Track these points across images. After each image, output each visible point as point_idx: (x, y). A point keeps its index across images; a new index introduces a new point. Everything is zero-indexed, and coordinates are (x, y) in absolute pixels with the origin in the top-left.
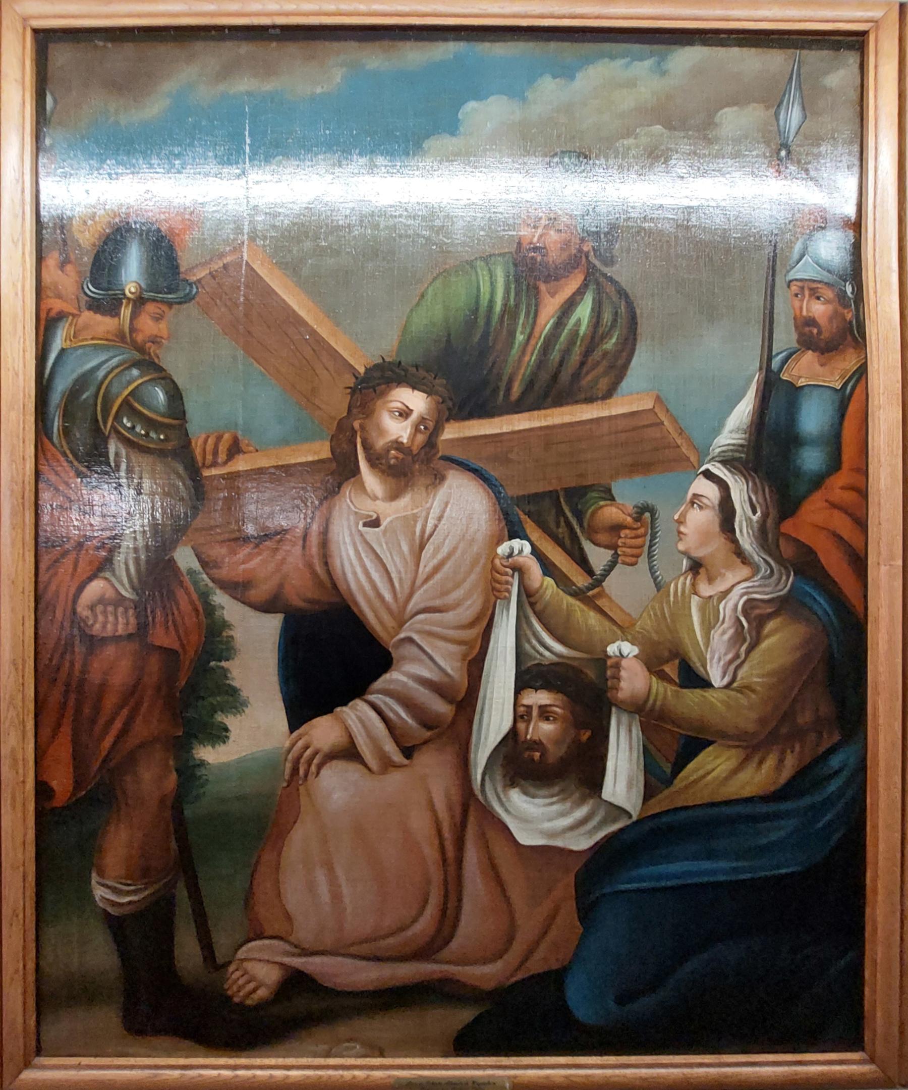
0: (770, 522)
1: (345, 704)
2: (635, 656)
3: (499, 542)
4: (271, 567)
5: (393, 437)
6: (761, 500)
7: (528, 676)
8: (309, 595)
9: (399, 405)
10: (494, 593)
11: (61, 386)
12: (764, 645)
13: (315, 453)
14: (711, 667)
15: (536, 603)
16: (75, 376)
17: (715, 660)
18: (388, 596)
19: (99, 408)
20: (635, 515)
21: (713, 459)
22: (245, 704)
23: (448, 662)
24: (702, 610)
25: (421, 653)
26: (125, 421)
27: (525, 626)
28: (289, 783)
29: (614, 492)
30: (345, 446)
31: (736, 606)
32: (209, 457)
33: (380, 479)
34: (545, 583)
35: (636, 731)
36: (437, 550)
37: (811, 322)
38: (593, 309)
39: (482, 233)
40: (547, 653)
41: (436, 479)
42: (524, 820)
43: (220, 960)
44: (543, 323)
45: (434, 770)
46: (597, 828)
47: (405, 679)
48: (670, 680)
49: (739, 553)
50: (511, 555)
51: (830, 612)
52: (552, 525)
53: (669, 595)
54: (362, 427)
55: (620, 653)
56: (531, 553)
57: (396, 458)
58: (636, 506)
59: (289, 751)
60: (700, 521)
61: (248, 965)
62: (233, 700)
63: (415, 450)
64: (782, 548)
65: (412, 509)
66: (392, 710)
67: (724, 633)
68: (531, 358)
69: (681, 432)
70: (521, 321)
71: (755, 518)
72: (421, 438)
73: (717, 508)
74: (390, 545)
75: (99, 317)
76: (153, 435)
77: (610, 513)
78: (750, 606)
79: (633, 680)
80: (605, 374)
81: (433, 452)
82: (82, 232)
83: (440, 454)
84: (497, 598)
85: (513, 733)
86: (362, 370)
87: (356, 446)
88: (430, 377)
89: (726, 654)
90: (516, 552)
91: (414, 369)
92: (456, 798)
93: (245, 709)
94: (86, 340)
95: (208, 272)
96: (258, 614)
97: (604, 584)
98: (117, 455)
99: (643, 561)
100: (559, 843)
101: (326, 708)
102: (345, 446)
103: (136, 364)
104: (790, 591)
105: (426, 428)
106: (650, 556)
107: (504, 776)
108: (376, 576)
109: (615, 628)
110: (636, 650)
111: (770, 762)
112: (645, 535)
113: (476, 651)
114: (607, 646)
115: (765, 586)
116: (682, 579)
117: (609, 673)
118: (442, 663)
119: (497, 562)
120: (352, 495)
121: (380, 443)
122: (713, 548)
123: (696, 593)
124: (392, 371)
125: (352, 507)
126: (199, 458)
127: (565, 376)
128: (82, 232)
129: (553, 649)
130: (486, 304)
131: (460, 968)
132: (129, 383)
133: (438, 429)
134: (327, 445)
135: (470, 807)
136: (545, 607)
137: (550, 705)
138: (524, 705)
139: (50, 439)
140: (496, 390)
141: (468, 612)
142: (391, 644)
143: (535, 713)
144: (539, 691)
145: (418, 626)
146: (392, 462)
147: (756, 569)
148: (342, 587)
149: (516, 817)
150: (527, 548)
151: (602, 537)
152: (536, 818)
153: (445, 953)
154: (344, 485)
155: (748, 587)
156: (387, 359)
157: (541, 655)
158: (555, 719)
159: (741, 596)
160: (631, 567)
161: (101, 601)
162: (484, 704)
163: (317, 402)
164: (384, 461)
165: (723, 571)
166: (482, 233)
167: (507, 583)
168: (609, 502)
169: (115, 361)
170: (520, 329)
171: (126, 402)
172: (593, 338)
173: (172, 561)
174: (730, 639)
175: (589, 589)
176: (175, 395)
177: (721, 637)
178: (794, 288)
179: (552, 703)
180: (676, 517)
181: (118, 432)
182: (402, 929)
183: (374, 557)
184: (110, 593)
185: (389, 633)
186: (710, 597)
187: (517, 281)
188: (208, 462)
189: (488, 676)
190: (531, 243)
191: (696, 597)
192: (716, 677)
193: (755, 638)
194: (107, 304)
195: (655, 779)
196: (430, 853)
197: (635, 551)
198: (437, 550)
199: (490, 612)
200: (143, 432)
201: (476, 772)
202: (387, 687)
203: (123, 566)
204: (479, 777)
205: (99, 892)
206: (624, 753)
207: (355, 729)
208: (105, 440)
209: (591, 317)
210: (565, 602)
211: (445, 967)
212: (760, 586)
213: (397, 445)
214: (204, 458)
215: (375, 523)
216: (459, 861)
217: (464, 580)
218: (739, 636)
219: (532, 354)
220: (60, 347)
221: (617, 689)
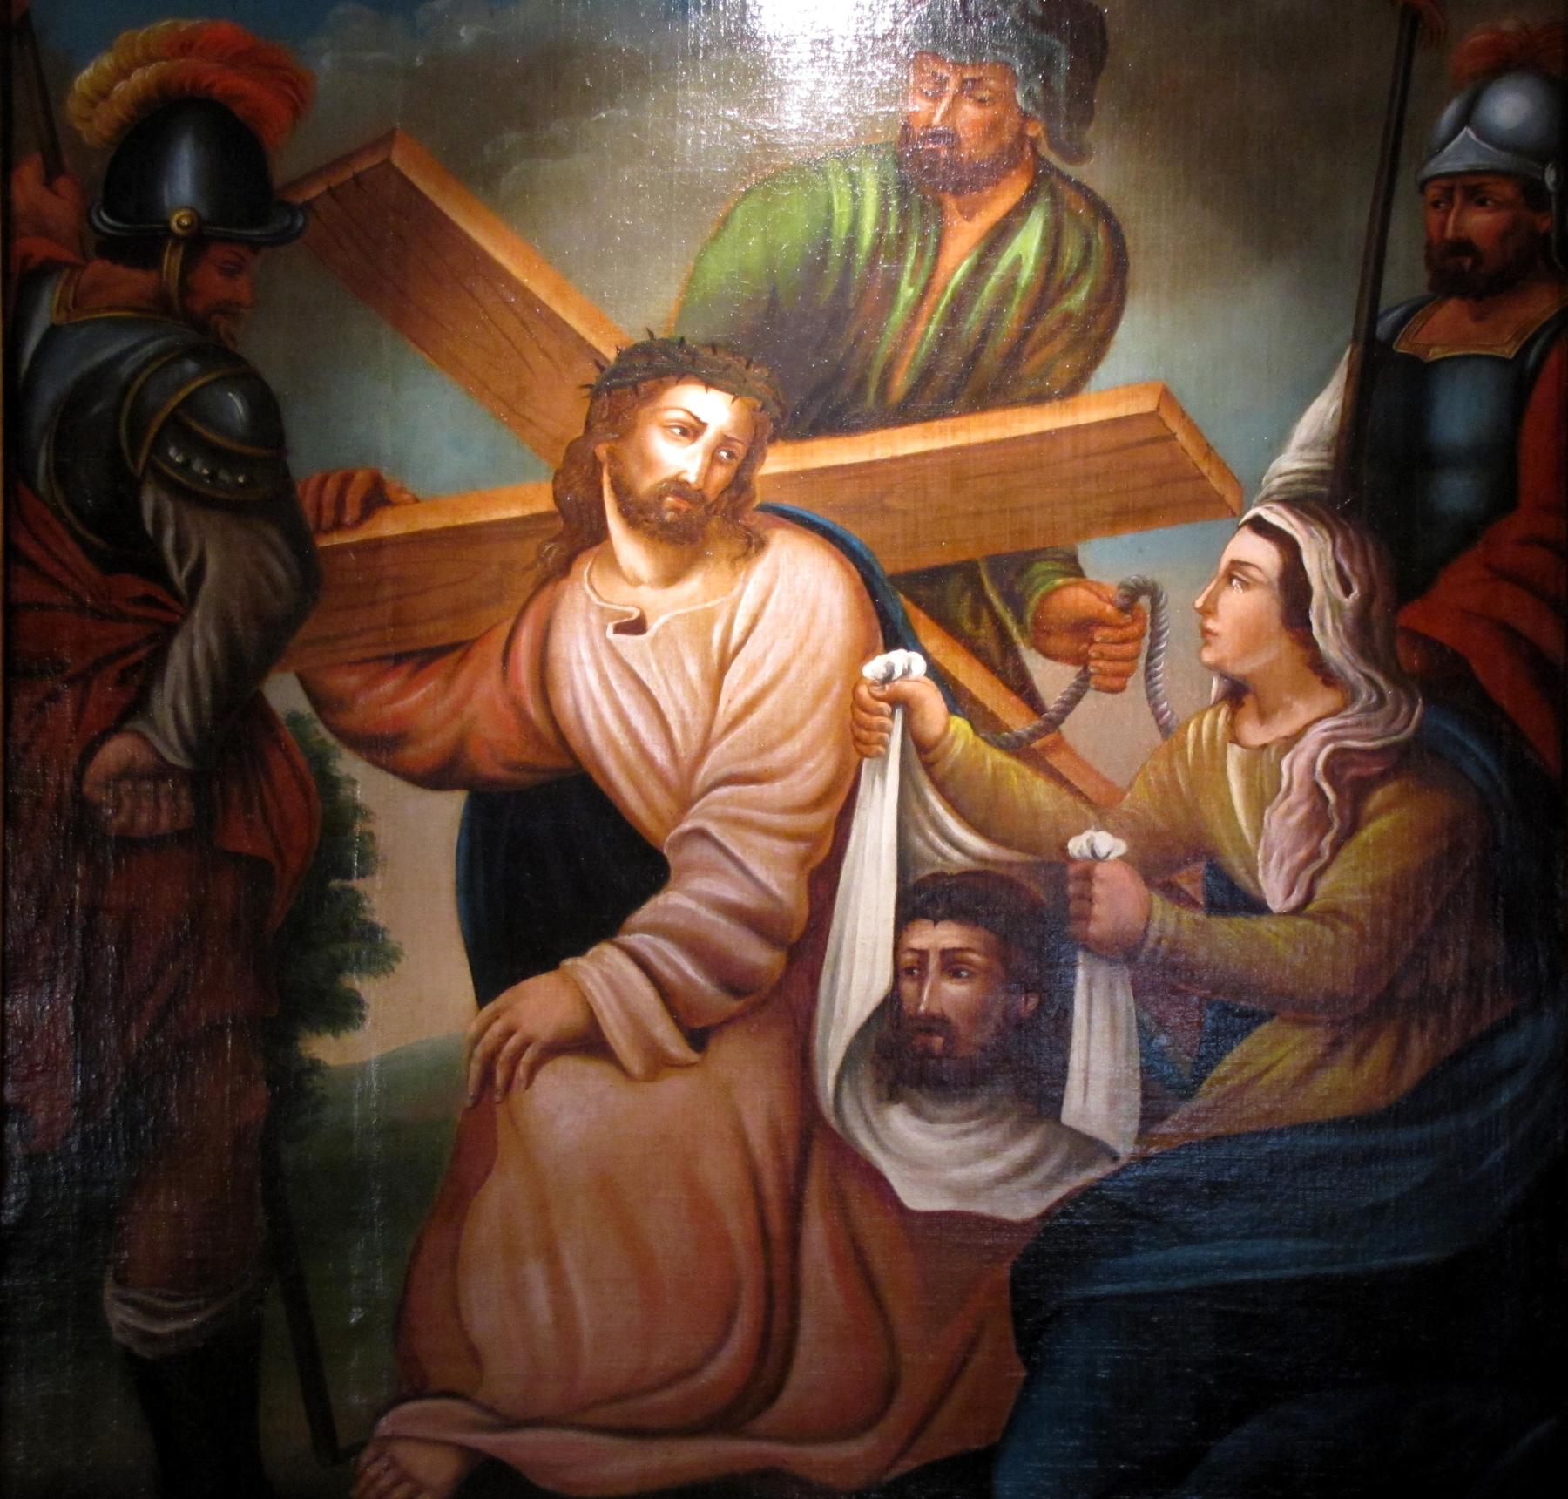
0: (1376, 609)
1: (580, 951)
2: (1121, 858)
3: (867, 654)
4: (443, 706)
5: (670, 472)
6: (1359, 568)
7: (919, 897)
8: (515, 757)
9: (680, 415)
10: (857, 743)
11: (49, 393)
12: (1367, 834)
13: (524, 504)
14: (1265, 874)
15: (932, 764)
16: (75, 374)
17: (1273, 862)
18: (660, 756)
19: (123, 430)
20: (1120, 601)
21: (1267, 498)
22: (395, 955)
23: (773, 874)
24: (1248, 770)
25: (721, 858)
26: (172, 452)
27: (915, 806)
28: (478, 1100)
29: (1082, 563)
30: (579, 489)
31: (1313, 761)
32: (328, 515)
33: (646, 545)
34: (953, 728)
35: (1124, 998)
36: (753, 670)
37: (1463, 246)
38: (1044, 240)
39: (836, 110)
40: (956, 855)
41: (750, 545)
42: (916, 1164)
43: (344, 1440)
44: (950, 266)
45: (745, 1074)
46: (1052, 1180)
47: (692, 905)
48: (1193, 903)
49: (1318, 666)
50: (888, 679)
51: (1495, 771)
52: (968, 626)
53: (1184, 746)
54: (612, 456)
55: (1093, 853)
56: (927, 675)
57: (676, 510)
58: (1122, 586)
59: (476, 1041)
60: (1241, 607)
61: (401, 1451)
62: (376, 951)
63: (711, 493)
64: (1402, 654)
65: (706, 601)
66: (669, 962)
67: (1290, 811)
68: (930, 329)
69: (1209, 452)
70: (909, 265)
71: (1348, 602)
72: (721, 474)
73: (1276, 584)
74: (666, 666)
75: (120, 271)
76: (224, 476)
77: (1076, 599)
78: (1338, 762)
79: (1118, 900)
80: (1068, 350)
81: (744, 497)
82: (88, 120)
83: (758, 502)
84: (863, 755)
85: (891, 1005)
86: (611, 355)
87: (601, 496)
88: (738, 364)
89: (1294, 850)
90: (898, 673)
91: (709, 352)
92: (787, 1125)
93: (394, 964)
94: (98, 310)
95: (323, 188)
96: (418, 792)
97: (1063, 727)
98: (158, 512)
99: (1136, 682)
100: (981, 1207)
101: (546, 961)
102: (581, 491)
103: (193, 352)
104: (1419, 729)
105: (731, 455)
106: (1149, 675)
107: (878, 1081)
108: (639, 720)
109: (1083, 808)
110: (1121, 847)
111: (1380, 1053)
112: (1137, 638)
113: (825, 850)
114: (1069, 839)
115: (1368, 724)
116: (1208, 718)
117: (1072, 889)
118: (761, 873)
119: (863, 691)
120: (594, 576)
121: (646, 484)
122: (1273, 657)
123: (1236, 740)
124: (668, 354)
125: (594, 598)
126: (310, 516)
127: (990, 360)
128: (88, 120)
129: (961, 844)
130: (843, 236)
131: (796, 1450)
132: (180, 386)
133: (753, 456)
134: (547, 488)
135: (812, 1136)
136: (953, 771)
137: (960, 950)
138: (913, 950)
139: (31, 485)
140: (860, 386)
141: (808, 783)
142: (673, 859)
143: (933, 963)
144: (940, 925)
145: (716, 809)
146: (669, 516)
147: (1350, 694)
148: (575, 741)
149: (899, 1158)
150: (918, 664)
151: (1061, 643)
152: (934, 1160)
153: (761, 1424)
154: (582, 557)
155: (1337, 728)
156: (659, 335)
157: (944, 856)
158: (971, 975)
159: (1324, 743)
160: (1109, 697)
161: (127, 773)
162: (839, 947)
163: (529, 412)
164: (652, 516)
165: (1288, 699)
166: (836, 110)
167: (882, 728)
168: (1072, 580)
169: (150, 349)
170: (906, 277)
171: (174, 420)
172: (1044, 288)
173: (260, 699)
174: (1301, 823)
175: (1034, 736)
176: (266, 407)
177: (1284, 822)
178: (1433, 192)
179: (966, 945)
180: (1199, 603)
181: (157, 472)
182: (693, 1371)
183: (634, 687)
184: (144, 758)
185: (661, 821)
186: (1264, 746)
187: (903, 195)
188: (326, 523)
189: (846, 905)
190: (928, 126)
191: (1237, 748)
192: (1274, 889)
193: (1348, 823)
194: (139, 242)
195: (1159, 1089)
196: (738, 1226)
197: (1121, 666)
198: (753, 670)
199: (851, 777)
200: (205, 471)
201: (825, 1075)
202: (659, 920)
203: (169, 711)
204: (830, 1084)
205: (120, 1316)
206: (1101, 1038)
207: (600, 1000)
208: (136, 487)
209: (1041, 254)
210: (989, 761)
211: (766, 1447)
212: (1358, 724)
213: (678, 486)
214: (319, 515)
215: (636, 627)
216: (794, 1241)
217: (803, 722)
218: (1317, 820)
219: (930, 320)
220: (47, 324)
221: (1086, 917)
